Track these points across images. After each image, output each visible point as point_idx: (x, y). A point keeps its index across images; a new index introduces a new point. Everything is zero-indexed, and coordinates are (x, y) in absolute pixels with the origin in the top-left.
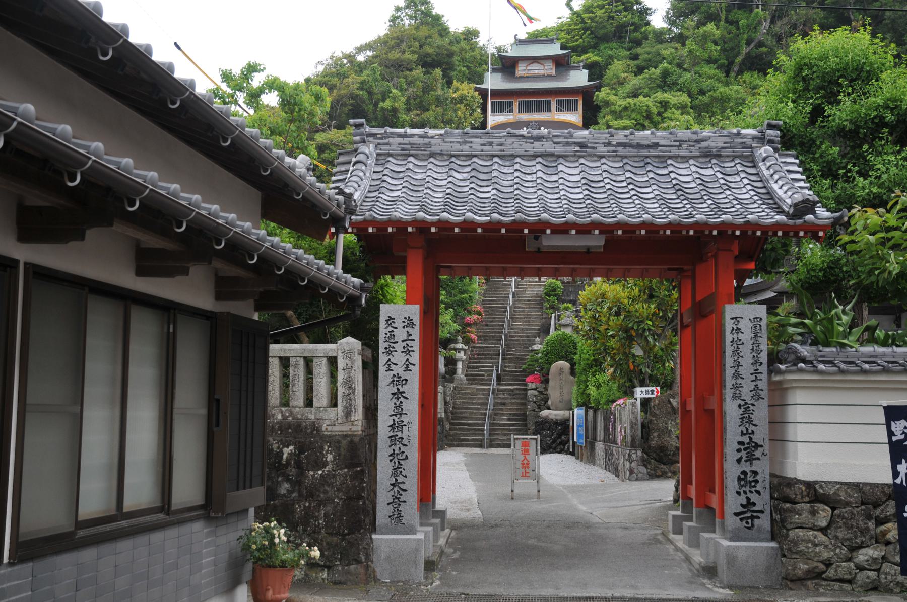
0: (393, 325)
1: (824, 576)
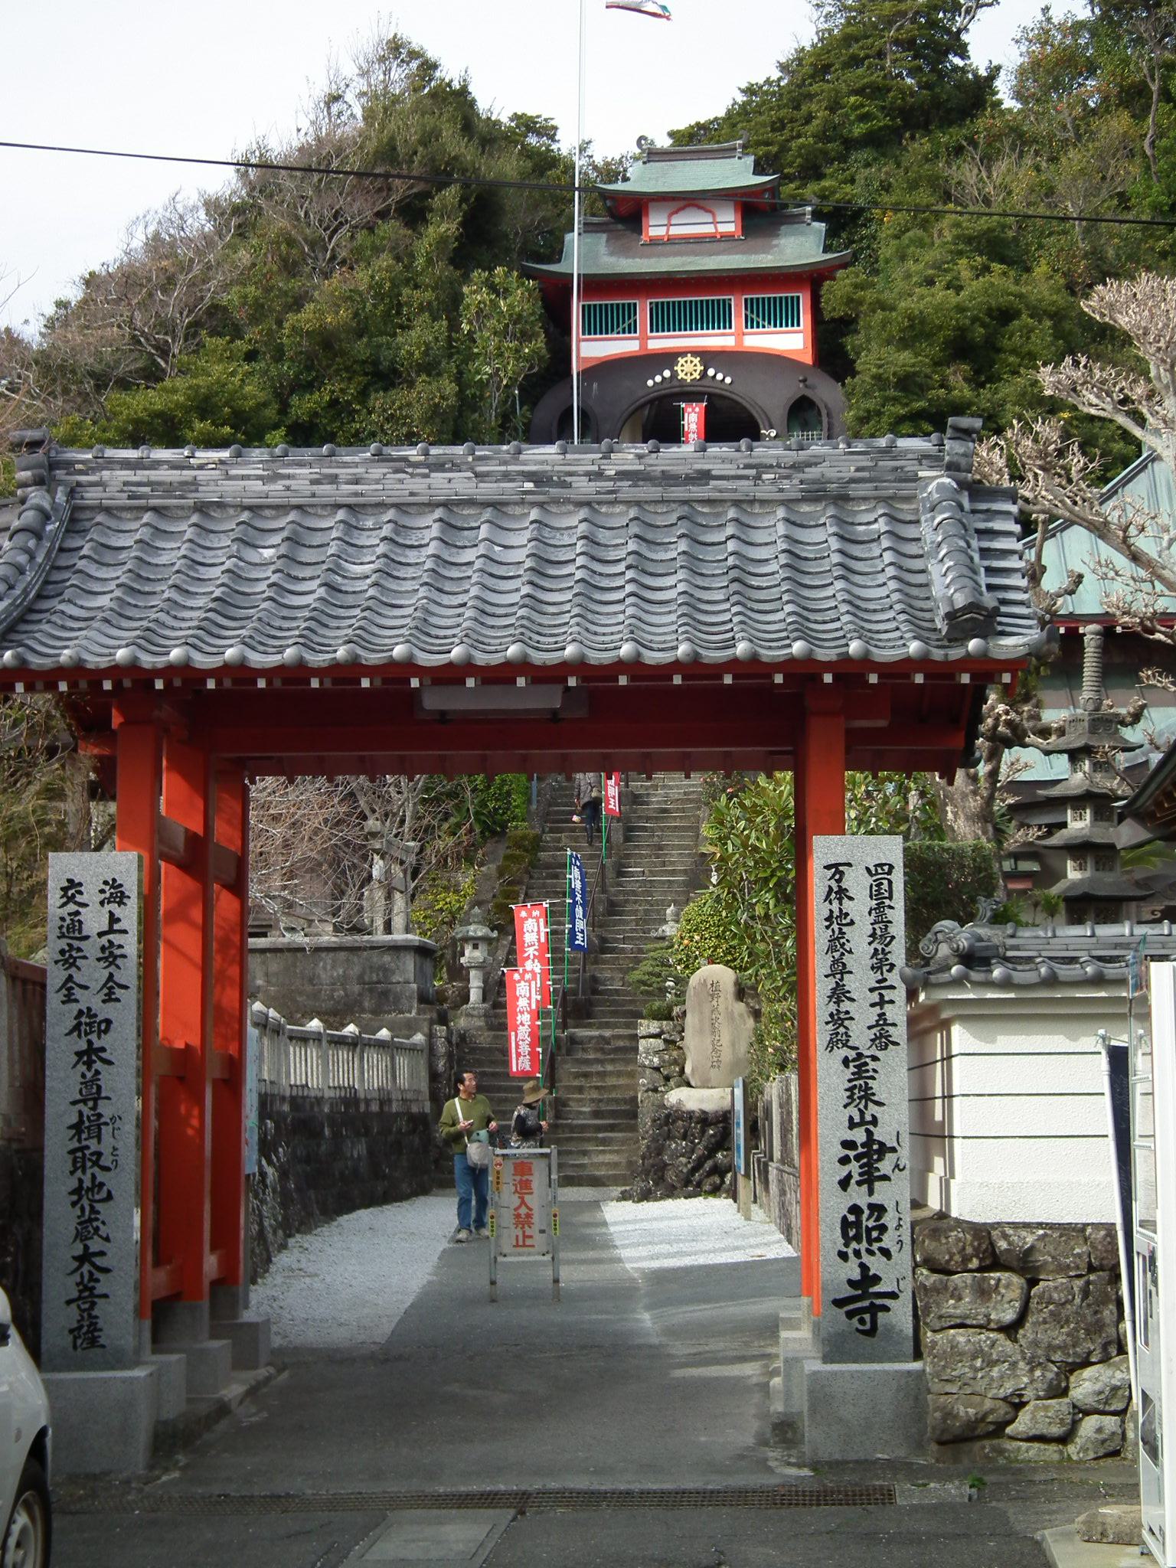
0: (78, 898)
1: (1009, 1430)
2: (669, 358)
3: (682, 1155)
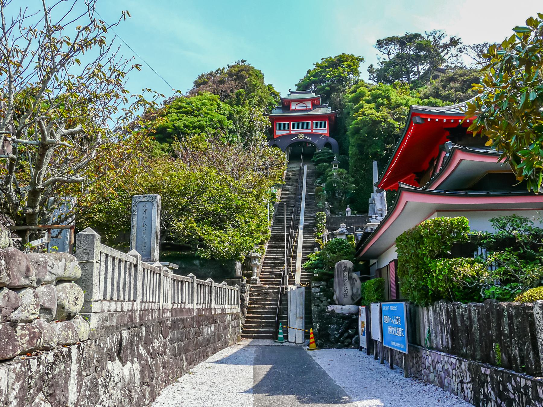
2: (297, 135)
3: (336, 331)
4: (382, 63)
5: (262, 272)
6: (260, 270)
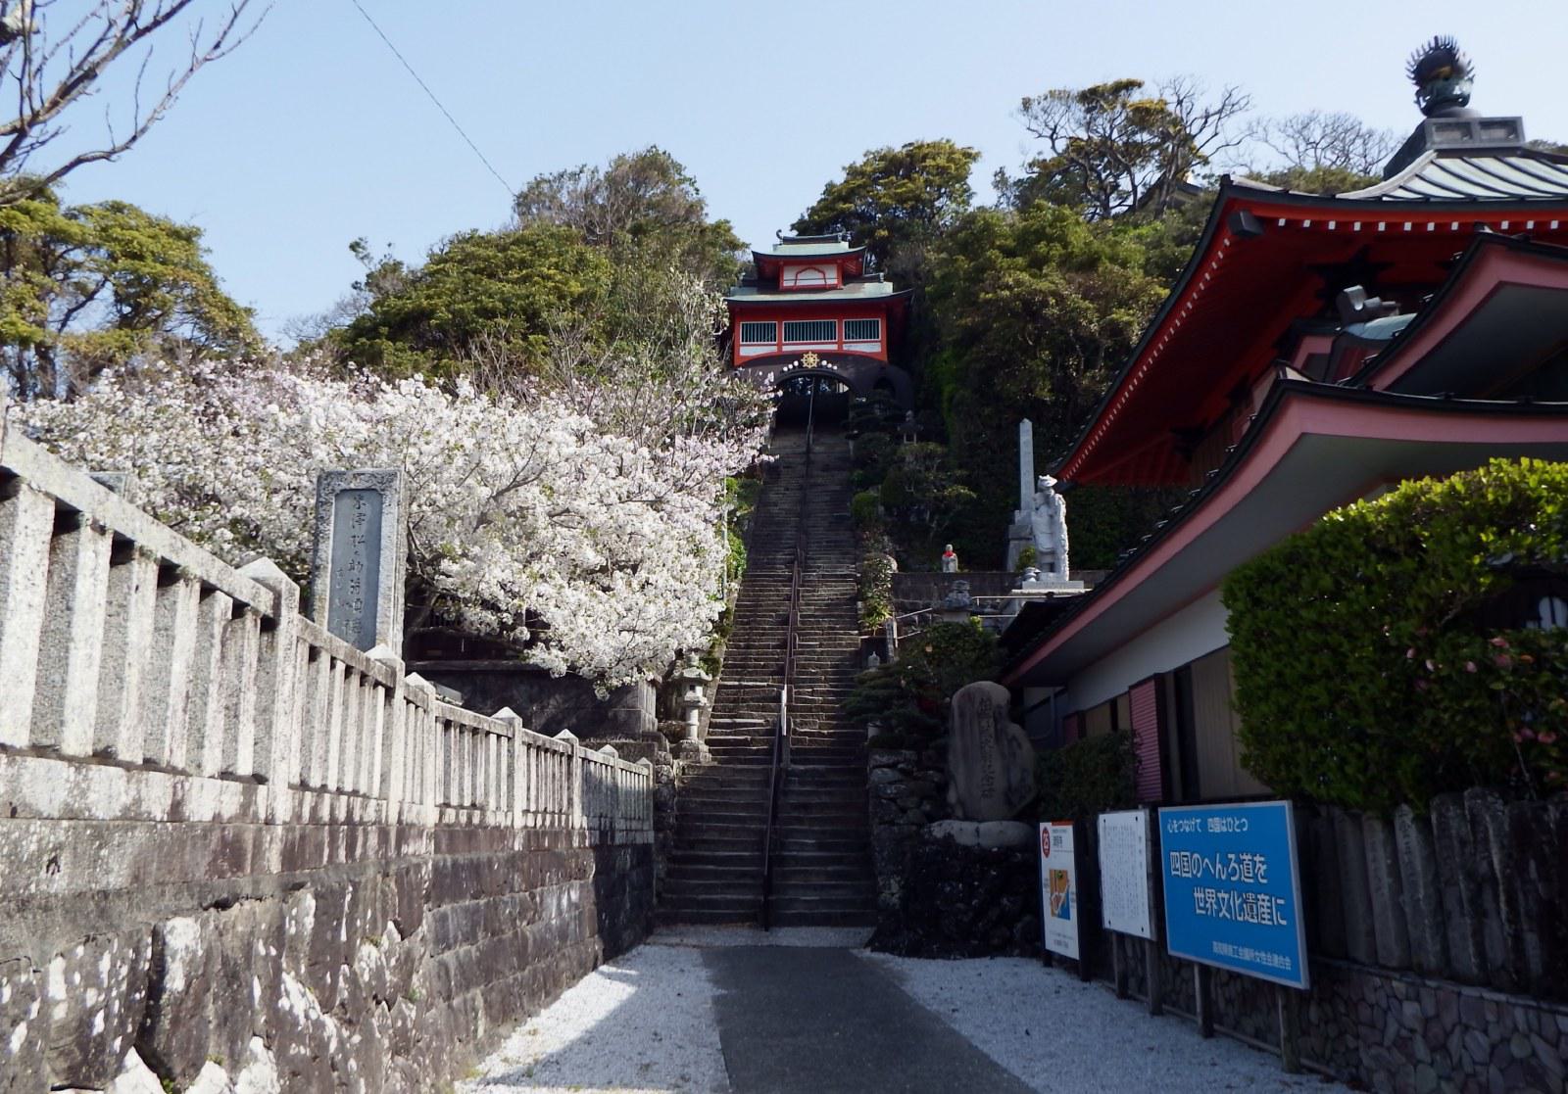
2: (798, 356)
4: (1031, 165)
5: (711, 725)
6: (706, 720)
